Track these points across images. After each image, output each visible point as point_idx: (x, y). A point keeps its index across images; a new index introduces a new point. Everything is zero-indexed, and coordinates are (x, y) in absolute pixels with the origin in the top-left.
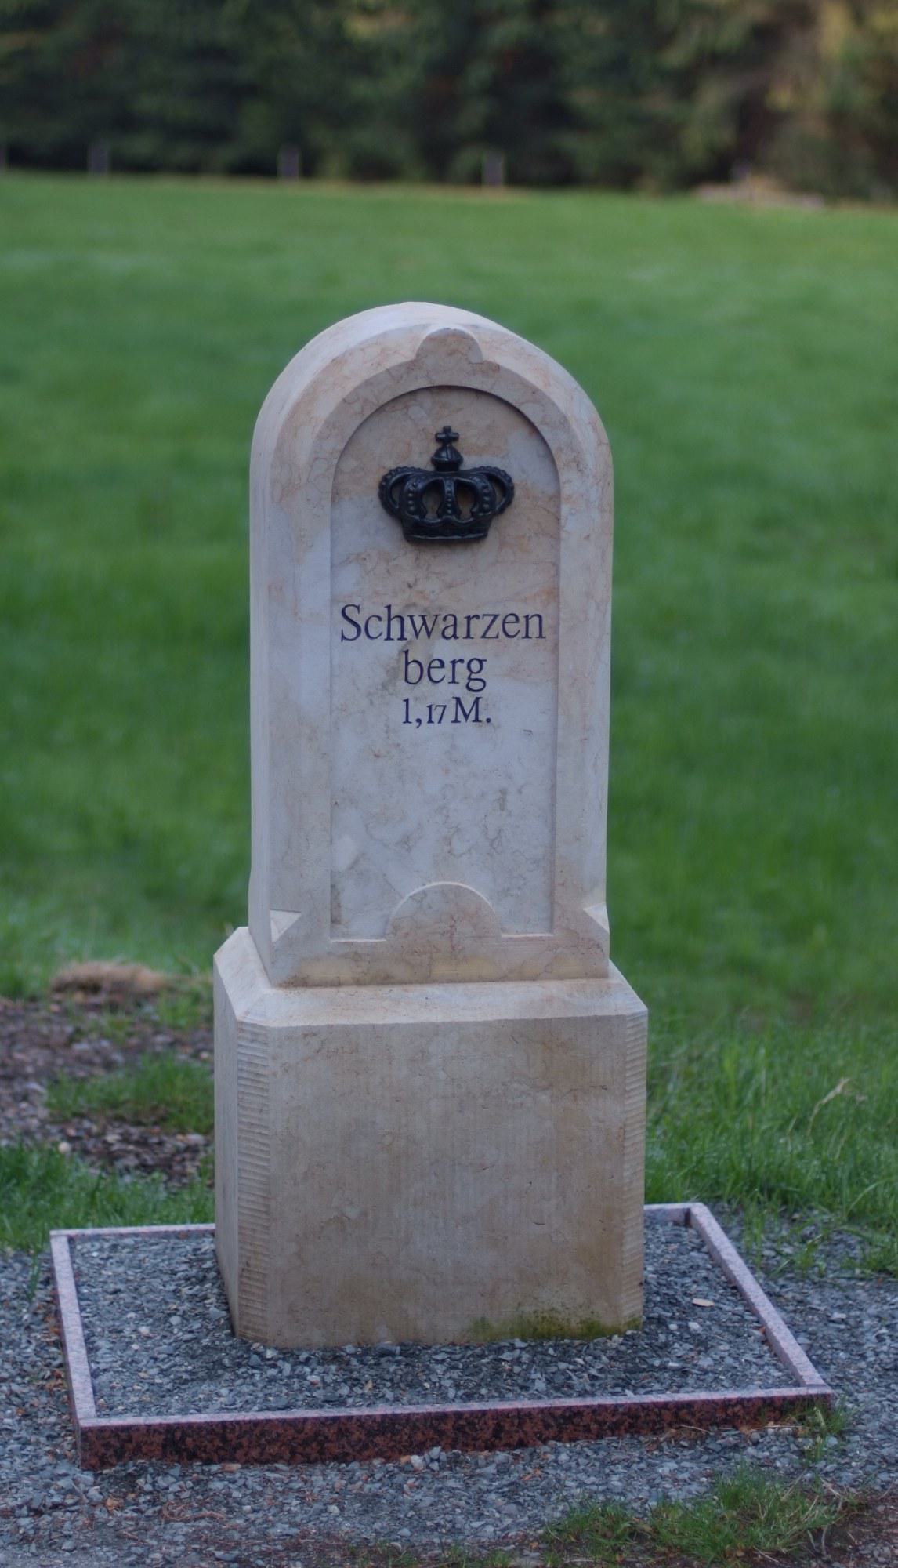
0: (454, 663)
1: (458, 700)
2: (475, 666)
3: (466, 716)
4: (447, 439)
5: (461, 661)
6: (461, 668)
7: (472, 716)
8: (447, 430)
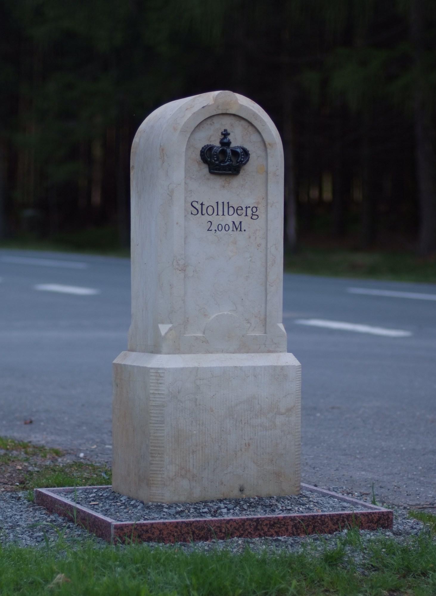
0: (246, 208)
1: (234, 222)
2: (254, 210)
3: (237, 229)
4: (225, 134)
5: (249, 207)
6: (249, 210)
7: (239, 229)
8: (225, 130)
